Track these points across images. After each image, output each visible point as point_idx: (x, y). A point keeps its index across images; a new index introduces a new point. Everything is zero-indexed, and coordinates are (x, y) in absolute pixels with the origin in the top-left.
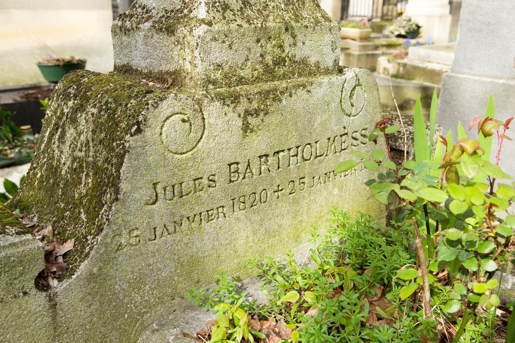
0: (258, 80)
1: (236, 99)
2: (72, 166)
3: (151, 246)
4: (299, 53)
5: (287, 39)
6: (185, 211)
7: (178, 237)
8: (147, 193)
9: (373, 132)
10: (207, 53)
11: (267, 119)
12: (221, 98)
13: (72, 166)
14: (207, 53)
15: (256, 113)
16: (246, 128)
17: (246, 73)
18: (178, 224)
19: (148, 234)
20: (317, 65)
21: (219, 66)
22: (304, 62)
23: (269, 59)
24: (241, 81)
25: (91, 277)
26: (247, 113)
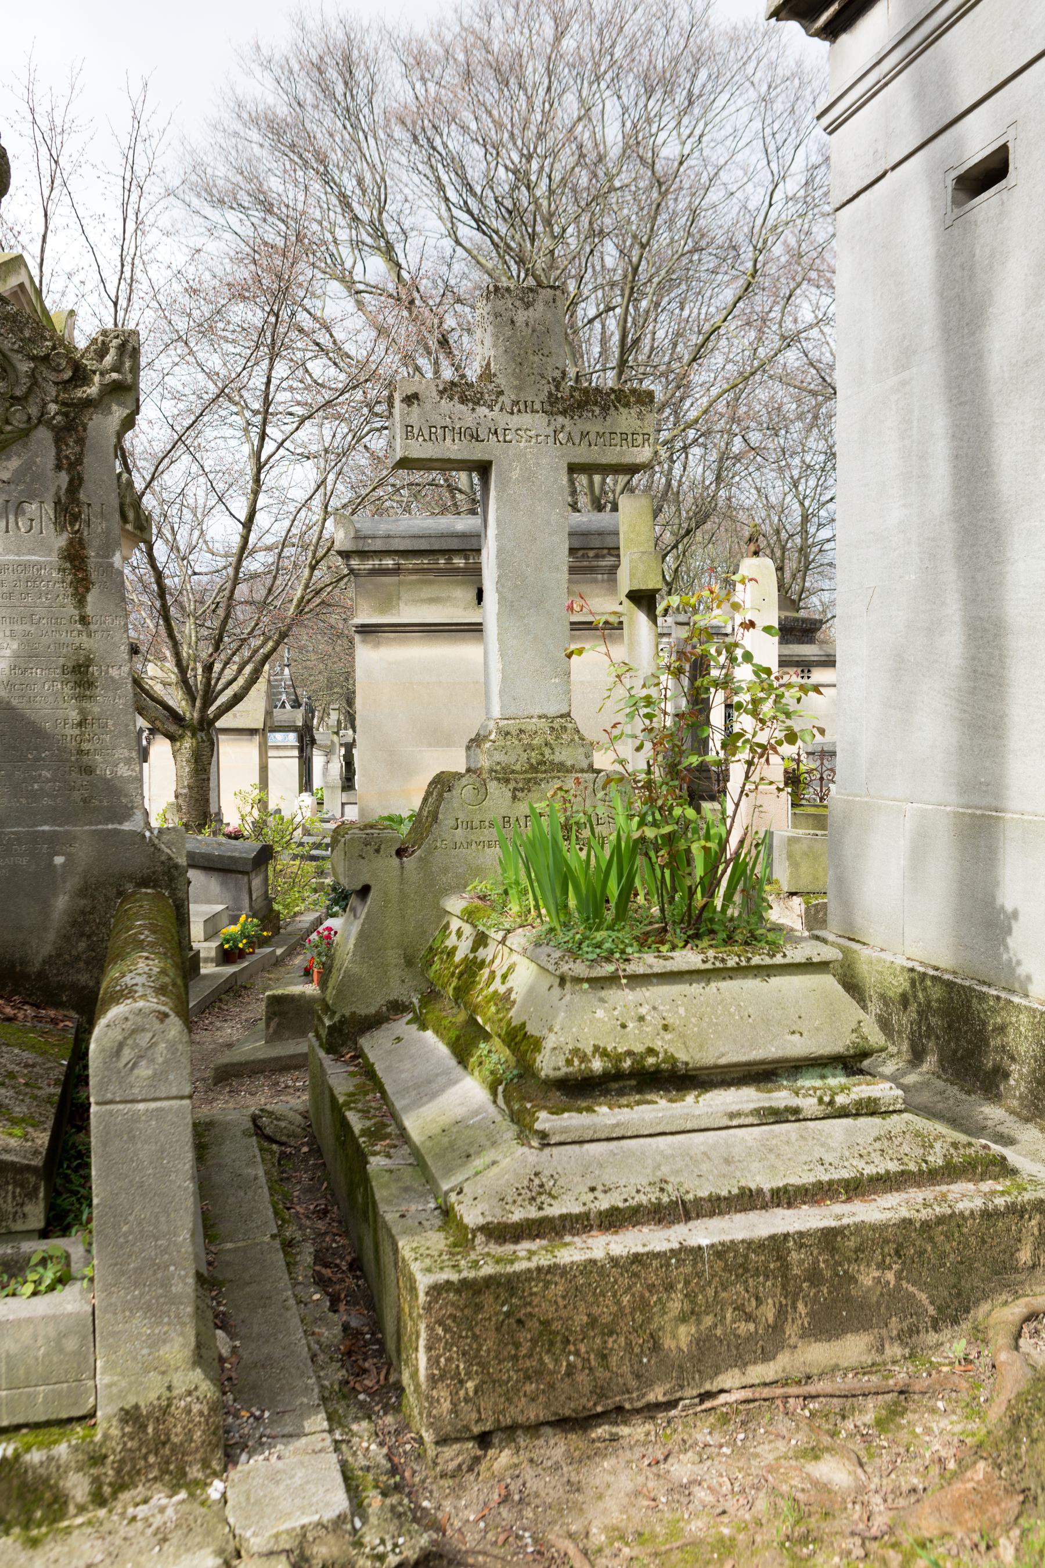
0: (526, 772)
1: (507, 781)
2: (47, 1534)
3: (453, 852)
4: (557, 758)
5: (547, 751)
6: (474, 838)
7: (469, 851)
8: (452, 822)
9: (273, 936)
10: (491, 756)
11: (530, 795)
12: (498, 779)
13: (47, 1534)
14: (491, 756)
15: (522, 790)
16: (514, 797)
17: (518, 767)
18: (469, 844)
19: (452, 845)
20: (573, 766)
21: (498, 763)
22: (562, 764)
23: (534, 761)
24: (513, 772)
25: (421, 859)
26: (515, 789)
